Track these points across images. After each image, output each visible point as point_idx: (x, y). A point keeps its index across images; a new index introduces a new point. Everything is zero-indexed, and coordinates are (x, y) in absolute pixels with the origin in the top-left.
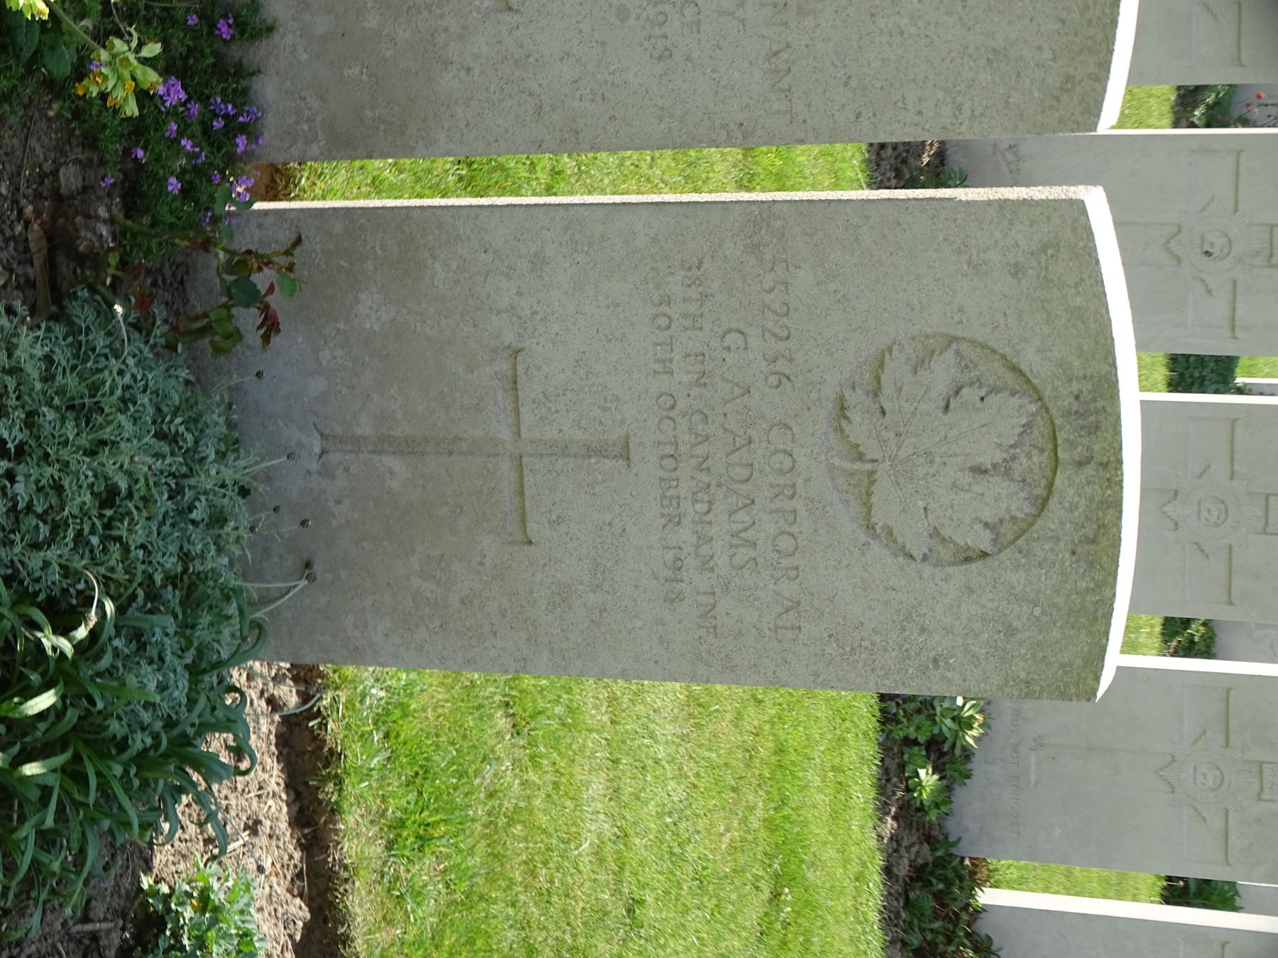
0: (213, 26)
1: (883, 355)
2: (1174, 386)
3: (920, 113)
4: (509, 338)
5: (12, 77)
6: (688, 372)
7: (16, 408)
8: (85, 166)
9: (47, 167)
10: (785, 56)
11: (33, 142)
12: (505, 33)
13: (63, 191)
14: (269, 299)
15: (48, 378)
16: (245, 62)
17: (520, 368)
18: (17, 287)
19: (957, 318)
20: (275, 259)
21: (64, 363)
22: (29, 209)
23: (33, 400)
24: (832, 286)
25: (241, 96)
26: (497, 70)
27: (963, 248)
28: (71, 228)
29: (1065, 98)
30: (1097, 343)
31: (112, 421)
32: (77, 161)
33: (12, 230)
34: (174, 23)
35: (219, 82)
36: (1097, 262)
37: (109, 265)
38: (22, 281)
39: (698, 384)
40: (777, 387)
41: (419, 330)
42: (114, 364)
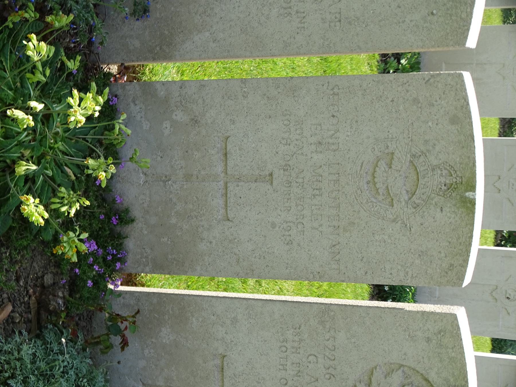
0: (110, 219)
1: (373, 370)
2: (493, 351)
3: (391, 274)
4: (221, 351)
5: (28, 240)
6: (293, 370)
7: (19, 375)
8: (55, 274)
9: (40, 274)
10: (337, 247)
11: (35, 264)
12: (226, 229)
13: (45, 284)
14: (125, 332)
15: (33, 362)
16: (121, 232)
17: (225, 363)
18: (24, 323)
19: (403, 357)
20: (128, 319)
21: (40, 357)
22: (31, 291)
23: (27, 372)
24: (353, 340)
25: (119, 247)
26: (222, 243)
27: (407, 329)
28: (47, 300)
29: (450, 272)
30: (460, 372)
31: (58, 381)
32: (52, 272)
33: (24, 299)
34: (95, 217)
35: (111, 240)
36: (461, 339)
37: (61, 317)
38: (26, 320)
39: (297, 375)
40: (329, 379)
41: (185, 345)
42: (61, 357)
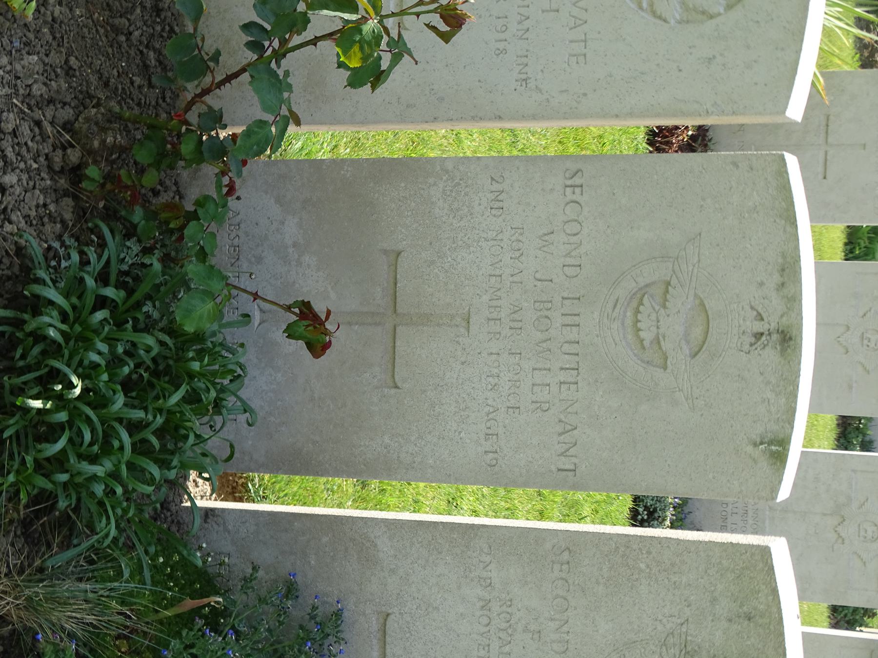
2: (835, 626)
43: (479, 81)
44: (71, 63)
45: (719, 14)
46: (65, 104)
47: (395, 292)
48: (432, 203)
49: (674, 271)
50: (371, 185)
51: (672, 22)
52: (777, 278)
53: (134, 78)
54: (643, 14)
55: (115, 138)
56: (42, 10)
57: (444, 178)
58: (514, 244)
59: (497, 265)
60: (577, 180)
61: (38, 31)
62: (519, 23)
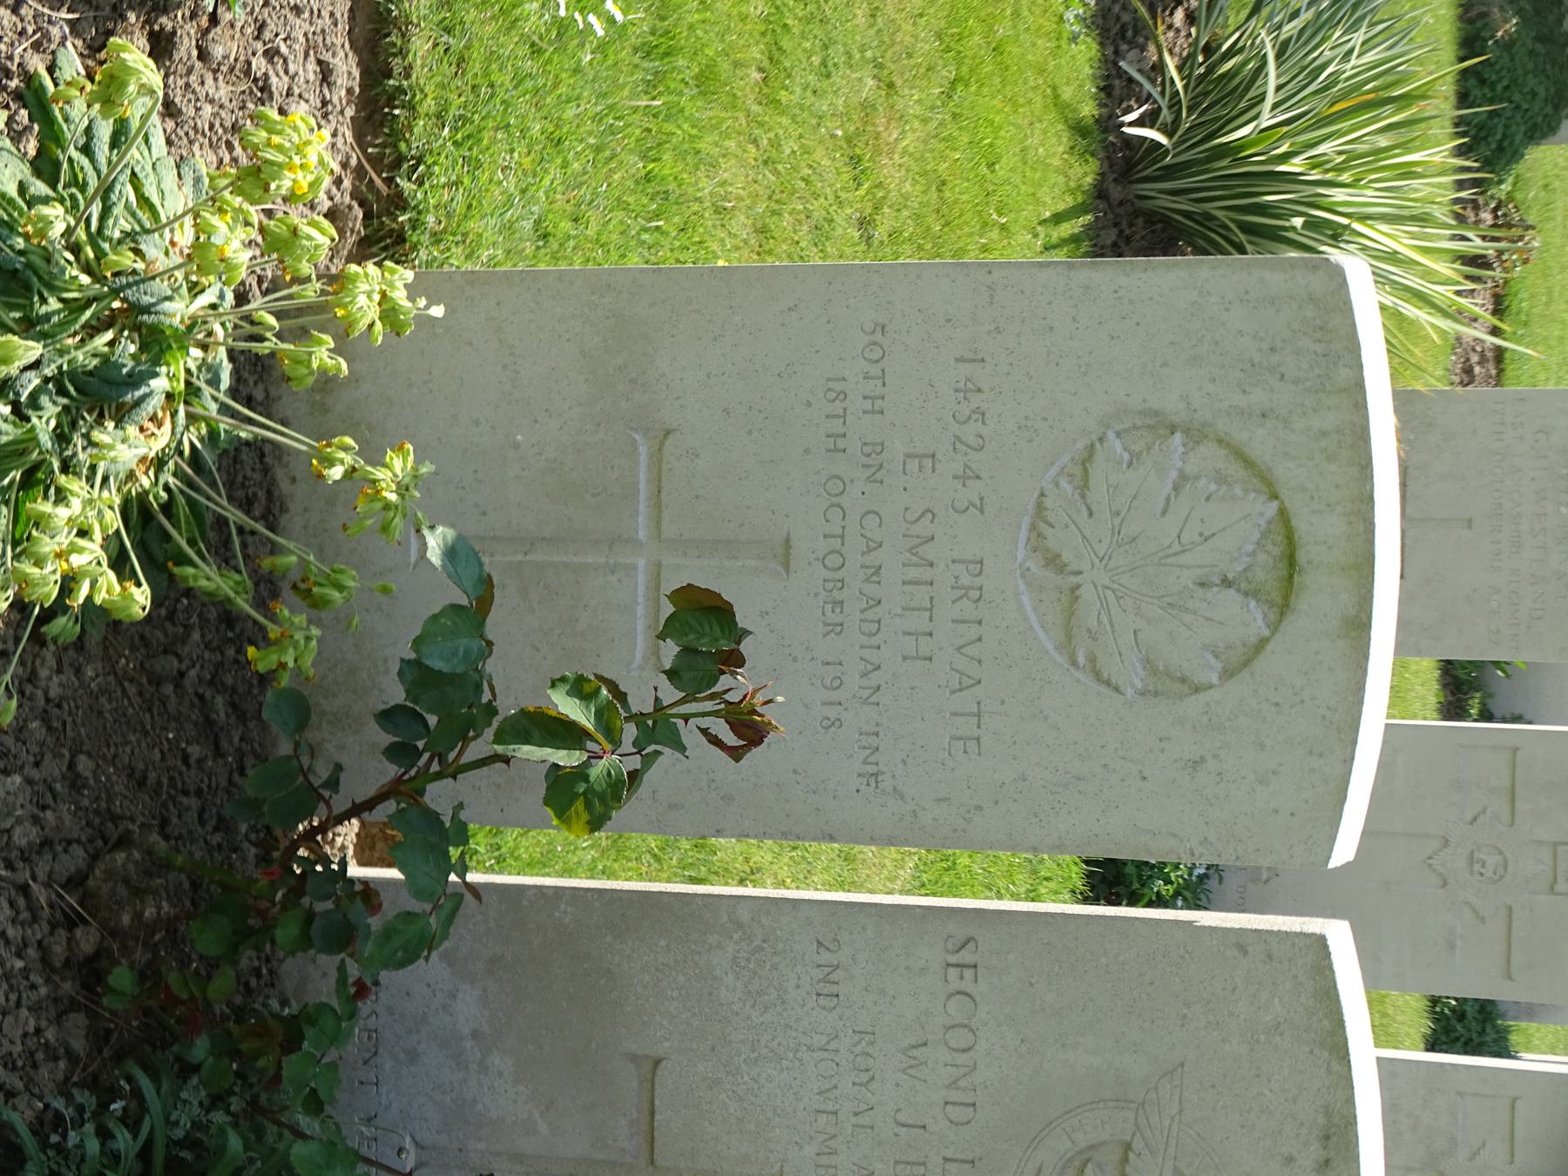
2: (1432, 1046)
43: (795, 772)
44: (80, 768)
45: (1211, 687)
46: (69, 842)
47: (652, 1129)
48: (715, 978)
49: (1137, 1125)
50: (608, 939)
51: (1130, 692)
52: (1315, 1152)
53: (189, 750)
54: (1078, 675)
55: (159, 908)
56: (29, 689)
57: (736, 936)
58: (859, 1059)
59: (831, 1095)
60: (966, 956)
61: (20, 730)
62: (864, 675)
